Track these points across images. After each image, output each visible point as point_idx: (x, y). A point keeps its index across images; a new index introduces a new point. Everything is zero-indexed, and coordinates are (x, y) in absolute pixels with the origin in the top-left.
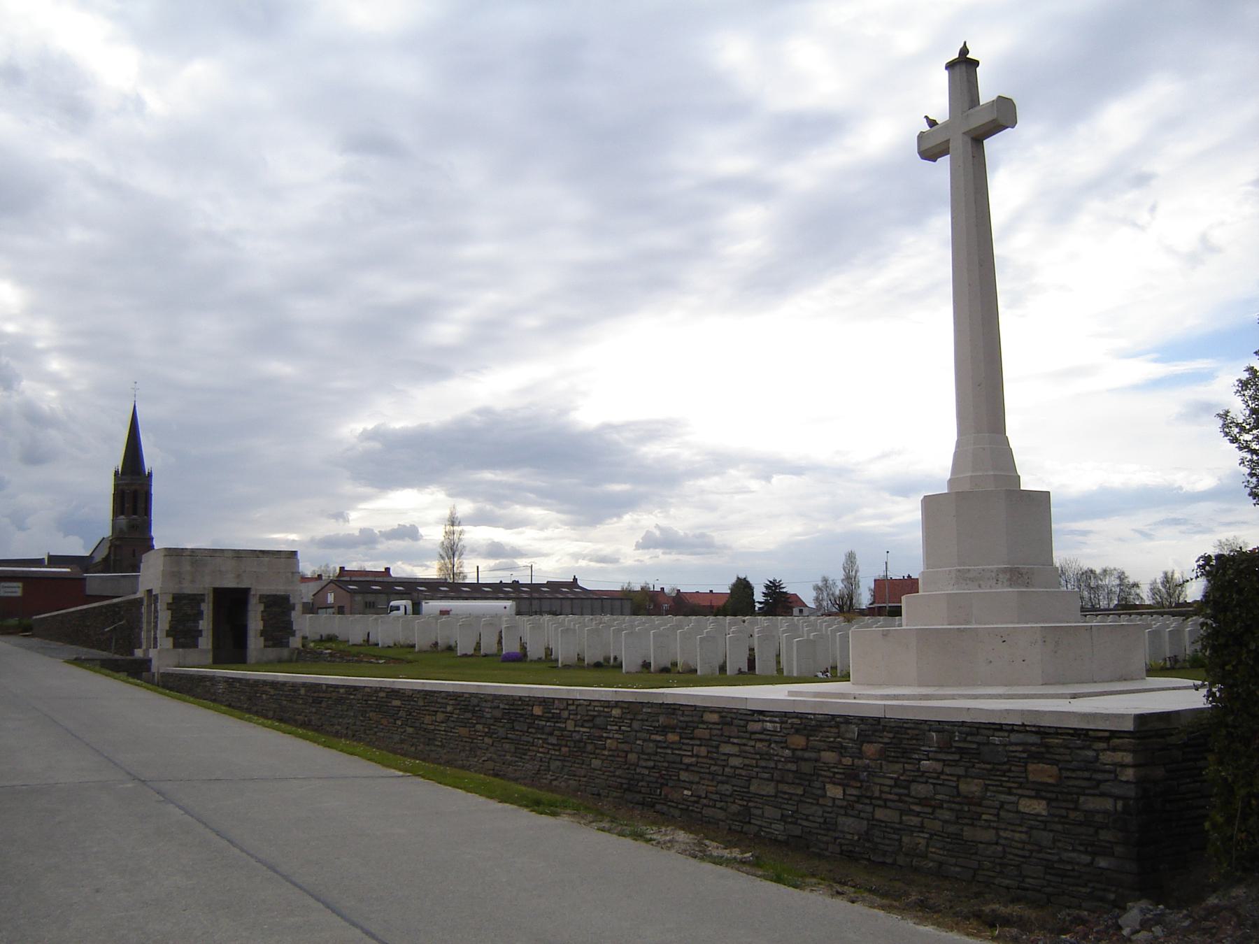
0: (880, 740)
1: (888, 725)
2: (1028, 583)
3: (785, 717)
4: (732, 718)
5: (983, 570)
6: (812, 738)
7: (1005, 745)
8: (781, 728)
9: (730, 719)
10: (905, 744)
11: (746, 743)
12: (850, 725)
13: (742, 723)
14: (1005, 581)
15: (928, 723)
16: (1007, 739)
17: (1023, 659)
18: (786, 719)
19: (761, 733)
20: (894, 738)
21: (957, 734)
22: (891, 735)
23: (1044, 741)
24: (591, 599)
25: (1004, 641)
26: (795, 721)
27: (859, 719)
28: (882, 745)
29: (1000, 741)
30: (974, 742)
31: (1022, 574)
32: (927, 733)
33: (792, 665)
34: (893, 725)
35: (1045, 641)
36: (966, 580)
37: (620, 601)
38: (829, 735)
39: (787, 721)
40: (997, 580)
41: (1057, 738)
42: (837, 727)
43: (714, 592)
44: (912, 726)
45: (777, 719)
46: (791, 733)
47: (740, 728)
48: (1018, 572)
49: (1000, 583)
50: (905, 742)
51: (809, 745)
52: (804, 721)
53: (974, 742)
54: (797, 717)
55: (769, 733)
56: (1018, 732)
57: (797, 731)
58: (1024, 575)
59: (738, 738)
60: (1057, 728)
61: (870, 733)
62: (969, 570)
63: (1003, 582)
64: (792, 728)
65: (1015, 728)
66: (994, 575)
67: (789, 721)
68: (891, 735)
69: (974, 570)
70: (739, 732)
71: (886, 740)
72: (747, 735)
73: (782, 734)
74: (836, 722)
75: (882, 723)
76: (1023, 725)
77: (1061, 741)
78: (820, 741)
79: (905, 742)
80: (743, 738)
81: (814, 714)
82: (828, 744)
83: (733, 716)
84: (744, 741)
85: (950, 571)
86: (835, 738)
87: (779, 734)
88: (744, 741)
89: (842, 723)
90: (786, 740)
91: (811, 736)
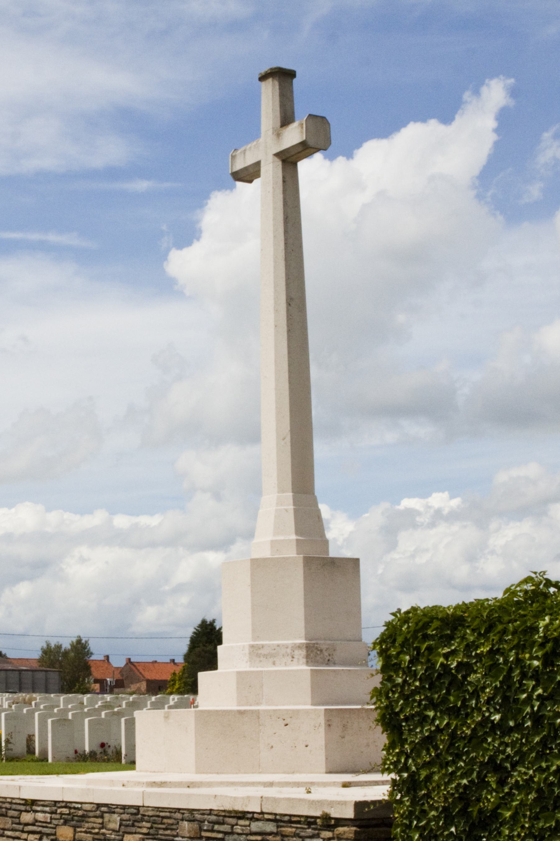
0: (139, 830)
1: (147, 814)
2: (329, 660)
3: (55, 806)
4: (6, 808)
5: (278, 646)
6: (78, 830)
7: (247, 835)
8: (51, 818)
9: (4, 810)
10: (161, 835)
11: (19, 836)
12: (113, 815)
13: (16, 813)
14: (301, 658)
15: (181, 811)
16: (248, 828)
17: (307, 744)
18: (56, 808)
19: (33, 825)
20: (151, 828)
21: (206, 823)
22: (149, 825)
23: (279, 829)
24: (6, 670)
25: (286, 725)
26: (66, 811)
27: (121, 808)
28: (141, 836)
29: (243, 830)
30: (219, 832)
31: (321, 651)
32: (180, 822)
33: (10, 746)
34: (150, 813)
35: (329, 725)
36: (260, 657)
37: (44, 673)
38: (95, 825)
39: (56, 810)
40: (293, 657)
41: (291, 827)
42: (102, 817)
43: (176, 661)
44: (168, 814)
45: (47, 809)
46: (60, 824)
47: (14, 819)
48: (317, 648)
49: (295, 660)
50: (161, 832)
51: (76, 837)
52: (72, 811)
53: (219, 832)
54: (66, 807)
55: (40, 824)
56: (258, 820)
57: (66, 822)
58: (324, 651)
59: (13, 830)
60: (290, 816)
61: (131, 823)
62: (263, 646)
63: (298, 659)
64: (61, 818)
65: (256, 816)
66: (289, 651)
67: (59, 811)
68: (149, 825)
69: (269, 646)
70: (12, 823)
71: (145, 831)
72: (21, 827)
73: (52, 826)
74: (101, 811)
75: (141, 812)
76: (262, 813)
77: (294, 830)
78: (86, 832)
79: (161, 832)
80: (16, 830)
81: (81, 803)
82: (92, 836)
83: (8, 806)
84: (17, 834)
85: (244, 647)
86: (100, 829)
87: (50, 825)
88: (17, 834)
89: (106, 812)
90: (56, 832)
91: (78, 827)
